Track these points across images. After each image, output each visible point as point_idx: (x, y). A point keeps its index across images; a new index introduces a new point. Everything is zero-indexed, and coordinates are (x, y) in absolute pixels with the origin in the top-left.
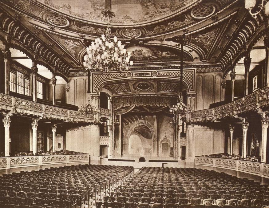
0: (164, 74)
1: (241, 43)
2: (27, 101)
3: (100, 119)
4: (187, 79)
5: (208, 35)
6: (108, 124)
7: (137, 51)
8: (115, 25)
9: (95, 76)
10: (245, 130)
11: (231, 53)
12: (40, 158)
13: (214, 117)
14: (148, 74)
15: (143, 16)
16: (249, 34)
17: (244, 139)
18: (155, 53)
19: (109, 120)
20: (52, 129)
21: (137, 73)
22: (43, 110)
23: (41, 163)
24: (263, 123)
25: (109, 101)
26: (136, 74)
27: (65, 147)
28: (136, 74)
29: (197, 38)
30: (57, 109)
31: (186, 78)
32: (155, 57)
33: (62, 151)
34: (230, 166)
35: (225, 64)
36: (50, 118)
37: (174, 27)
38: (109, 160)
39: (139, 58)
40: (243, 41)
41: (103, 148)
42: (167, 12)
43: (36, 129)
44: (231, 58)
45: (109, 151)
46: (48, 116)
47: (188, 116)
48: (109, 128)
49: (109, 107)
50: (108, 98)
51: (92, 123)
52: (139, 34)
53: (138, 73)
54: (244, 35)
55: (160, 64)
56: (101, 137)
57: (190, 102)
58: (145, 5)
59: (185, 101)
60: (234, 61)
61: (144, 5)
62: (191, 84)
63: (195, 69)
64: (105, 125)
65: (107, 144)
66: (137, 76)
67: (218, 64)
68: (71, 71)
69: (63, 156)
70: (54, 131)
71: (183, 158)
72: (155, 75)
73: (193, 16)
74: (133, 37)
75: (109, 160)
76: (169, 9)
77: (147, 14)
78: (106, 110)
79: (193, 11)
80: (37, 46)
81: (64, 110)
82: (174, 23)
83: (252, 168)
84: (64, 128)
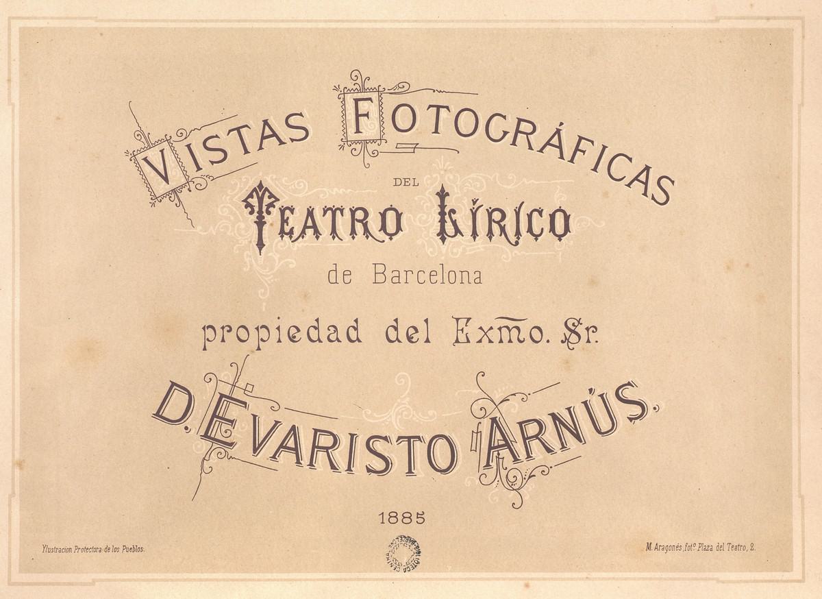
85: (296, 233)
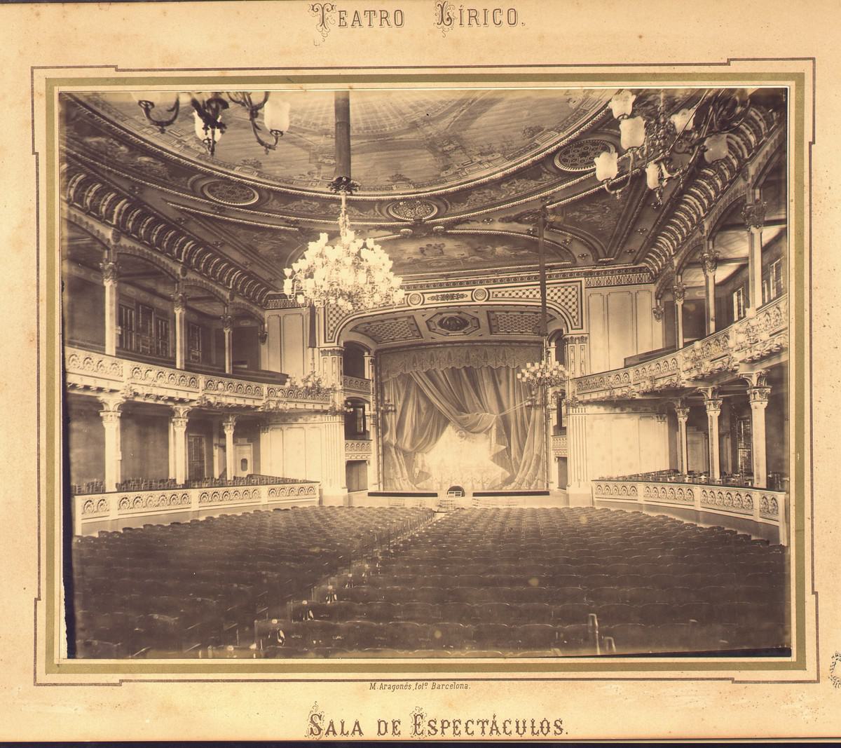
0: (503, 295)
1: (691, 219)
2: (161, 368)
3: (346, 402)
4: (563, 304)
5: (603, 204)
6: (367, 412)
7: (430, 248)
8: (370, 196)
9: (573, 289)
10: (713, 413)
11: (671, 241)
12: (194, 493)
13: (633, 387)
14: (462, 296)
15: (437, 173)
16: (709, 197)
17: (712, 435)
18: (476, 250)
19: (369, 402)
20: (223, 427)
21: (435, 295)
22: (265, 392)
23: (195, 506)
24: (752, 397)
25: (367, 360)
26: (433, 298)
27: (260, 469)
28: (433, 298)
29: (577, 214)
30: (236, 382)
31: (559, 301)
32: (478, 258)
33: (250, 476)
34: (689, 501)
35: (658, 266)
36: (218, 403)
37: (516, 193)
38: (371, 494)
39: (438, 262)
40: (696, 213)
41: (353, 466)
42: (495, 162)
43: (184, 429)
44: (670, 253)
45: (371, 474)
46: (212, 400)
47: (570, 388)
48: (369, 421)
49: (369, 373)
50: (366, 354)
51: (325, 412)
52: (432, 210)
53: (438, 296)
54: (696, 201)
55: (493, 272)
56: (350, 442)
57: (572, 355)
58: (440, 149)
59: (561, 358)
60: (678, 258)
61: (437, 151)
62: (574, 314)
63: (583, 279)
64: (360, 415)
65: (364, 458)
66: (435, 301)
67: (640, 265)
68: (270, 297)
69: (251, 488)
70: (229, 432)
71: (563, 485)
72: (415, 302)
73: (561, 167)
74: (417, 218)
75: (371, 494)
76: (500, 155)
77: (447, 168)
78: (360, 380)
79: (560, 156)
80: (185, 247)
81: (254, 385)
82: (517, 184)
83: (744, 503)
84: (253, 425)
85: (350, 733)
